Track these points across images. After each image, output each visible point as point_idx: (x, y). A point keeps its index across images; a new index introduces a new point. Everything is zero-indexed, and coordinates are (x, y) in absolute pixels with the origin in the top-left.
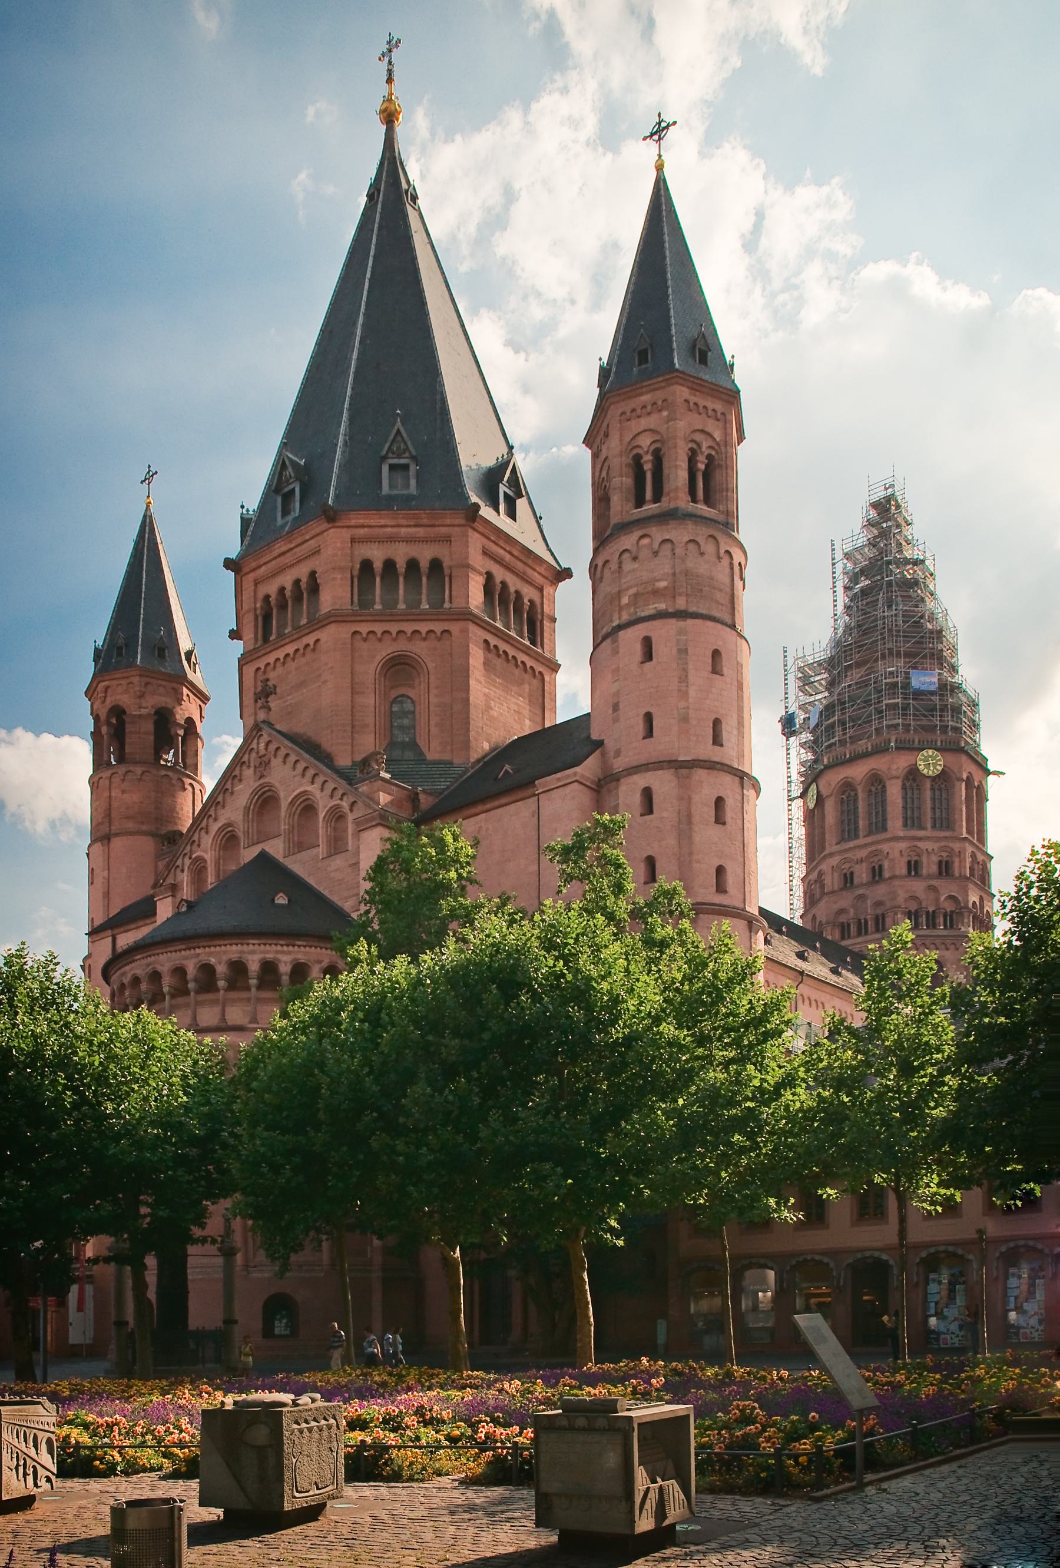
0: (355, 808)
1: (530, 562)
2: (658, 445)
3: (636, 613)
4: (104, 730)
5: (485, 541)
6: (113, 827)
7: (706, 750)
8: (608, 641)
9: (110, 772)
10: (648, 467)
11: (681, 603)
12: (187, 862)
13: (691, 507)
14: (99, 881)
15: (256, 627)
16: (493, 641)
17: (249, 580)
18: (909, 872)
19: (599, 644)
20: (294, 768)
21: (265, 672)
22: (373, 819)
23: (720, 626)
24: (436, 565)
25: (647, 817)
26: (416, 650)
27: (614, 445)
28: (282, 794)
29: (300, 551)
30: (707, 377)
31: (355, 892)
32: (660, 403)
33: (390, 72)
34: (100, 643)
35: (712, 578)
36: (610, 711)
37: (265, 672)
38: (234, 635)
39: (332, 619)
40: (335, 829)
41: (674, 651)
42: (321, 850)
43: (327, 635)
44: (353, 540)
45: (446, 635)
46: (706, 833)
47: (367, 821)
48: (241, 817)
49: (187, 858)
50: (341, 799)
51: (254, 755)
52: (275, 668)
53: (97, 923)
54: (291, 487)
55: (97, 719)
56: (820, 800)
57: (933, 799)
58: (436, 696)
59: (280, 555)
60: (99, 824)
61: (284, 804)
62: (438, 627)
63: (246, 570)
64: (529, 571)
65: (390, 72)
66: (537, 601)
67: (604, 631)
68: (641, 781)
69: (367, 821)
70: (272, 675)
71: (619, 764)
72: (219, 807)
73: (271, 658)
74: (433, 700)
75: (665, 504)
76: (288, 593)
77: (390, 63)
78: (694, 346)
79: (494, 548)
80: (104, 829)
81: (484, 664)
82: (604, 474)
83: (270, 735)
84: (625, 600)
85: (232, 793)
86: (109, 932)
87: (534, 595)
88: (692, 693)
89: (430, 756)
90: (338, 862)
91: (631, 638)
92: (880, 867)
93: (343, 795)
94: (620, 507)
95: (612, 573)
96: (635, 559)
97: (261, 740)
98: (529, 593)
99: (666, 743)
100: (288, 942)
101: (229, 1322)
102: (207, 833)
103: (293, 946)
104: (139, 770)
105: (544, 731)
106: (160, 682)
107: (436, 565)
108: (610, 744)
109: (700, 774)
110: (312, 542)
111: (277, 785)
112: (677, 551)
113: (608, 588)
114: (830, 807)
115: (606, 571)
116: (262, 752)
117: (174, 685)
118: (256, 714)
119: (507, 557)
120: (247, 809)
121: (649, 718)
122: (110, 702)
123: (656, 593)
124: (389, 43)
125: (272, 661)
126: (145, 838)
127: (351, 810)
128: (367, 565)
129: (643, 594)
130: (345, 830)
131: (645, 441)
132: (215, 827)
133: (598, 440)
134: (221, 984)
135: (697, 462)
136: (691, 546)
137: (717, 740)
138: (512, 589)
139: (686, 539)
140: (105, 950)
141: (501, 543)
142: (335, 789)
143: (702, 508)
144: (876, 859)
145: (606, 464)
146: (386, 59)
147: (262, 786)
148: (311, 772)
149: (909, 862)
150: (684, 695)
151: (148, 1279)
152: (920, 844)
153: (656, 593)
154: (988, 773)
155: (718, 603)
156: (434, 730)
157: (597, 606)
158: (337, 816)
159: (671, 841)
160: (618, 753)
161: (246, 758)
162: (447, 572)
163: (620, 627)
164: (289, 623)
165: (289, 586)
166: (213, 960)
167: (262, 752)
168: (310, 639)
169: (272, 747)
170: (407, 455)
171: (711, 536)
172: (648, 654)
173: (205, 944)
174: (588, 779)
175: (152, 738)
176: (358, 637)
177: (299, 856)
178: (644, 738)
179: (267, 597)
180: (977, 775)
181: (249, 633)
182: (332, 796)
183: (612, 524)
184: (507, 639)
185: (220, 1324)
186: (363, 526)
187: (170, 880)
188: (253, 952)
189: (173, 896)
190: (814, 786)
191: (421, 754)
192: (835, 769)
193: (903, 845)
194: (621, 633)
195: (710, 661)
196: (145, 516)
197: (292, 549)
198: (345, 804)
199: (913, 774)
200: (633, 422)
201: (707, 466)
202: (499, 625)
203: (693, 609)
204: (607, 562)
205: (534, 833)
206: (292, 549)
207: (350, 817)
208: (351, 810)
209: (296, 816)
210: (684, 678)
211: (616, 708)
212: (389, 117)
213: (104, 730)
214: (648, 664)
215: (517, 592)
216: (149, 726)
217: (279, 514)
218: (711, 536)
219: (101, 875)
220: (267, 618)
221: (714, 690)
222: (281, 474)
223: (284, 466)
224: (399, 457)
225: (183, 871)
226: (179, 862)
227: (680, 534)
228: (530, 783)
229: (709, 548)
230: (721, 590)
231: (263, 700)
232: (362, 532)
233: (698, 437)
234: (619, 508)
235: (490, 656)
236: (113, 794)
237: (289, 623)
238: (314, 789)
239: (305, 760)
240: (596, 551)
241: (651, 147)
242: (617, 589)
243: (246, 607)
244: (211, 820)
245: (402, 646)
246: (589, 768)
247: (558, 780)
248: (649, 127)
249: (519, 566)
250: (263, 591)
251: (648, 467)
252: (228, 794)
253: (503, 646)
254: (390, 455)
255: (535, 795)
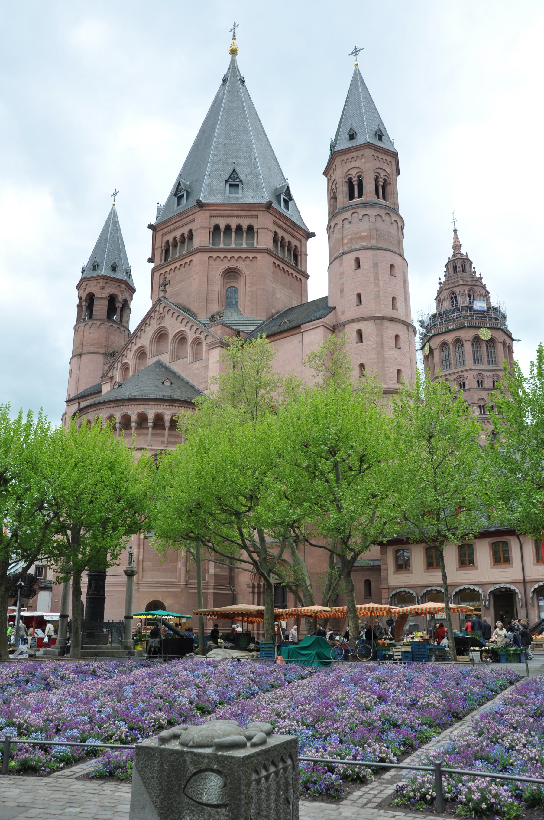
0: (207, 338)
1: (295, 229)
2: (360, 174)
3: (351, 247)
4: (84, 304)
5: (274, 217)
6: (83, 350)
7: (388, 312)
8: (338, 260)
9: (85, 323)
10: (355, 183)
11: (374, 242)
12: (120, 365)
13: (377, 200)
14: (74, 376)
15: (161, 255)
16: (277, 263)
17: (159, 235)
18: (479, 386)
19: (332, 262)
20: (177, 319)
21: (164, 275)
22: (216, 343)
23: (393, 254)
24: (250, 228)
25: (359, 344)
26: (241, 266)
27: (339, 175)
28: (170, 332)
29: (184, 221)
30: (382, 146)
31: (205, 380)
32: (360, 156)
33: (234, 36)
34: (85, 264)
35: (388, 232)
36: (339, 292)
37: (164, 275)
38: (150, 260)
39: (199, 250)
40: (196, 349)
41: (371, 265)
42: (189, 360)
43: (197, 258)
44: (211, 216)
45: (255, 259)
46: (391, 353)
47: (214, 344)
48: (148, 343)
49: (119, 363)
50: (200, 334)
51: (157, 313)
52: (169, 273)
53: (72, 396)
54: (182, 194)
55: (80, 299)
56: (431, 351)
57: (488, 352)
58: (249, 287)
59: (175, 223)
60: (77, 348)
61: (171, 337)
62: (251, 255)
63: (158, 230)
64: (295, 233)
65: (234, 36)
66: (299, 246)
67: (335, 256)
68: (356, 326)
69: (214, 344)
70: (167, 276)
71: (343, 318)
72: (138, 338)
73: (168, 269)
74: (247, 289)
75: (363, 199)
76: (178, 240)
77: (234, 33)
78: (376, 134)
79: (278, 221)
80: (79, 351)
81: (273, 273)
82: (334, 187)
83: (165, 303)
84: (346, 241)
85: (145, 331)
86: (77, 401)
87: (297, 243)
88: (381, 284)
89: (246, 315)
90: (197, 365)
91: (349, 259)
92: (464, 383)
93: (201, 332)
94: (342, 199)
95: (339, 229)
96: (350, 222)
97: (161, 306)
98: (294, 242)
99: (367, 308)
100: (170, 404)
101: (128, 617)
102: (131, 351)
103: (173, 406)
104: (98, 323)
105: (302, 305)
106: (112, 282)
107: (250, 228)
108: (339, 310)
109: (387, 324)
110: (191, 216)
111: (168, 327)
112: (371, 219)
113: (337, 235)
114: (436, 353)
115: (336, 228)
116: (161, 311)
117: (119, 284)
118: (159, 295)
119: (285, 226)
120: (152, 339)
121: (359, 296)
122: (87, 291)
123: (362, 238)
124: (234, 25)
125: (168, 270)
126: (99, 355)
127: (205, 339)
128: (217, 228)
129: (354, 238)
130: (202, 349)
131: (354, 172)
132: (135, 348)
133: (330, 173)
134: (133, 425)
135: (379, 181)
136: (378, 218)
137: (394, 307)
138: (286, 240)
139: (375, 214)
140: (75, 407)
141: (282, 219)
142: (197, 329)
143: (382, 201)
144: (461, 379)
145: (335, 182)
146: (233, 31)
147: (160, 328)
148: (185, 321)
149: (478, 381)
150: (377, 285)
151: (82, 590)
152: (482, 372)
153: (362, 238)
154: (513, 340)
155: (391, 243)
156: (247, 303)
157: (331, 244)
158: (197, 342)
159: (373, 356)
160: (343, 313)
161: (153, 315)
162: (255, 231)
163: (344, 253)
164: (178, 253)
165: (178, 237)
166: (130, 413)
167: (161, 311)
168: (188, 260)
169: (167, 309)
170: (238, 180)
171: (387, 213)
172: (358, 265)
173: (126, 404)
174: (328, 325)
175: (106, 308)
176: (211, 259)
177: (177, 362)
178: (357, 305)
179: (167, 242)
180: (508, 341)
181: (157, 258)
182: (195, 333)
183: (338, 208)
184: (284, 262)
185: (122, 619)
186: (216, 210)
187: (110, 374)
188: (151, 409)
189: (111, 382)
190: (427, 344)
191: (241, 314)
192: (438, 336)
193: (475, 373)
194: (344, 256)
195: (389, 269)
196: (112, 210)
197: (181, 220)
198: (202, 336)
199: (477, 339)
200: (347, 164)
201: (384, 183)
202: (280, 255)
203: (380, 245)
204: (336, 224)
205: (301, 352)
206: (181, 220)
207: (204, 343)
208: (205, 339)
209: (177, 342)
210: (376, 277)
211: (342, 291)
212: (233, 52)
213: (84, 304)
214: (358, 270)
215: (289, 242)
216: (106, 302)
217: (176, 205)
218: (387, 213)
219: (76, 372)
220: (167, 251)
221: (392, 283)
222: (177, 188)
223: (179, 184)
224: (234, 181)
225: (117, 369)
226: (115, 365)
227: (372, 212)
228: (299, 327)
229: (386, 218)
230: (393, 238)
231: (163, 287)
232: (215, 212)
233: (379, 171)
234: (342, 200)
235: (275, 269)
236: (85, 334)
237: (178, 253)
238: (187, 329)
239: (183, 315)
240: (330, 221)
241: (353, 57)
242: (341, 236)
243: (157, 246)
244: (133, 345)
245: (233, 264)
246: (329, 319)
247: (313, 325)
248: (352, 50)
249: (290, 230)
250: (165, 239)
251: (355, 183)
252: (142, 332)
253: (282, 265)
254: (230, 180)
255: (301, 332)
